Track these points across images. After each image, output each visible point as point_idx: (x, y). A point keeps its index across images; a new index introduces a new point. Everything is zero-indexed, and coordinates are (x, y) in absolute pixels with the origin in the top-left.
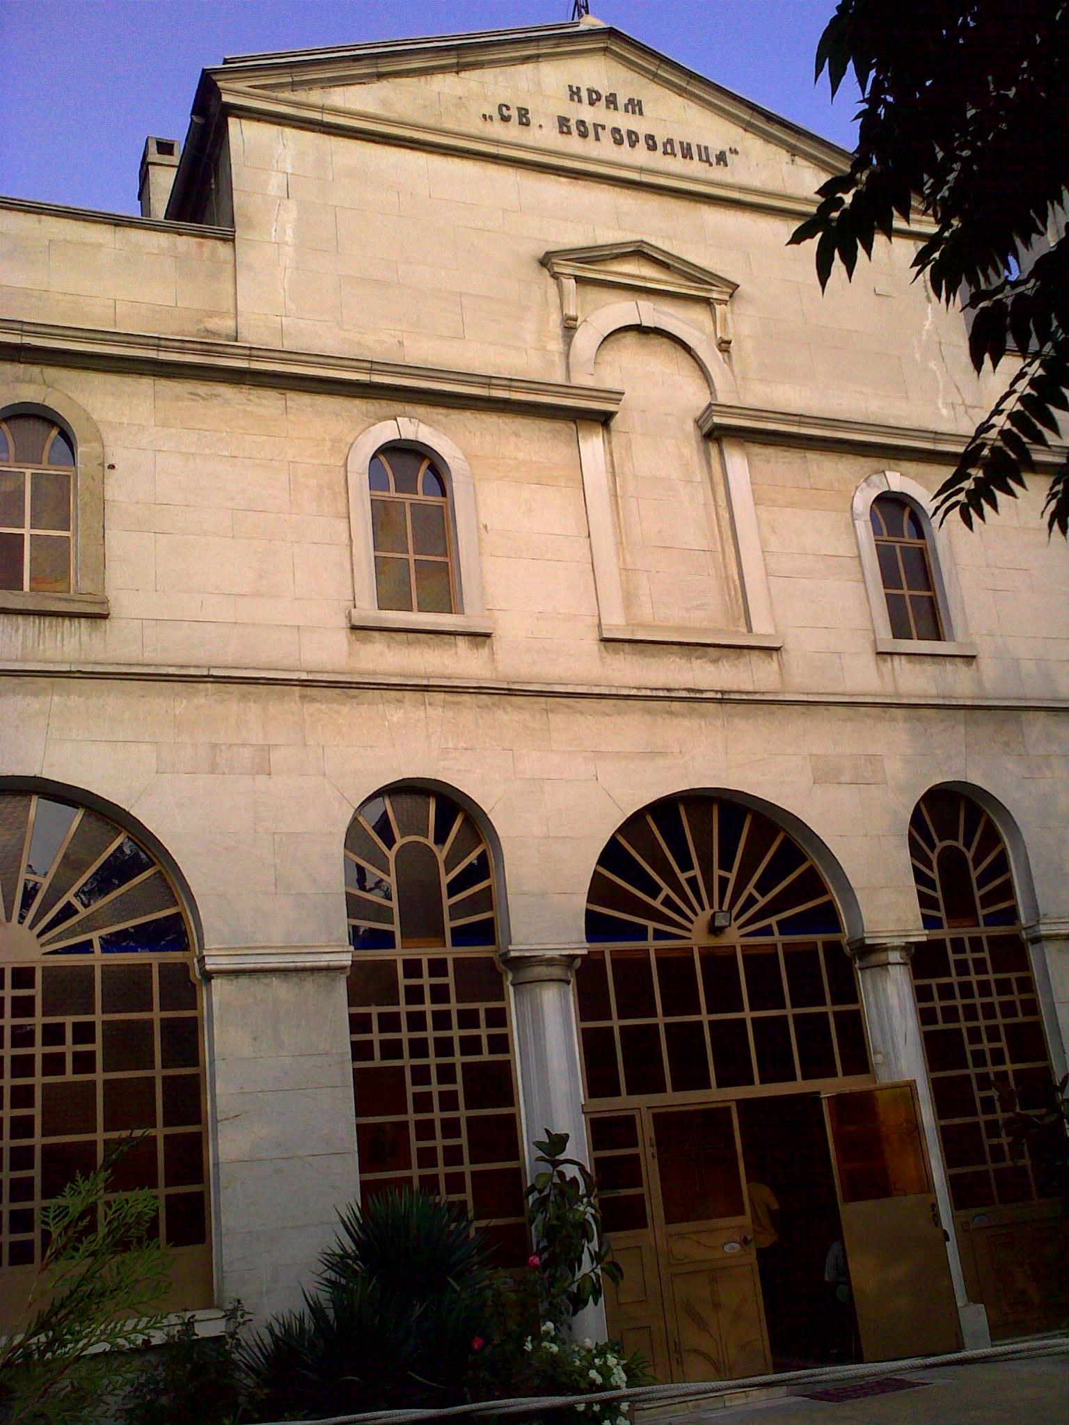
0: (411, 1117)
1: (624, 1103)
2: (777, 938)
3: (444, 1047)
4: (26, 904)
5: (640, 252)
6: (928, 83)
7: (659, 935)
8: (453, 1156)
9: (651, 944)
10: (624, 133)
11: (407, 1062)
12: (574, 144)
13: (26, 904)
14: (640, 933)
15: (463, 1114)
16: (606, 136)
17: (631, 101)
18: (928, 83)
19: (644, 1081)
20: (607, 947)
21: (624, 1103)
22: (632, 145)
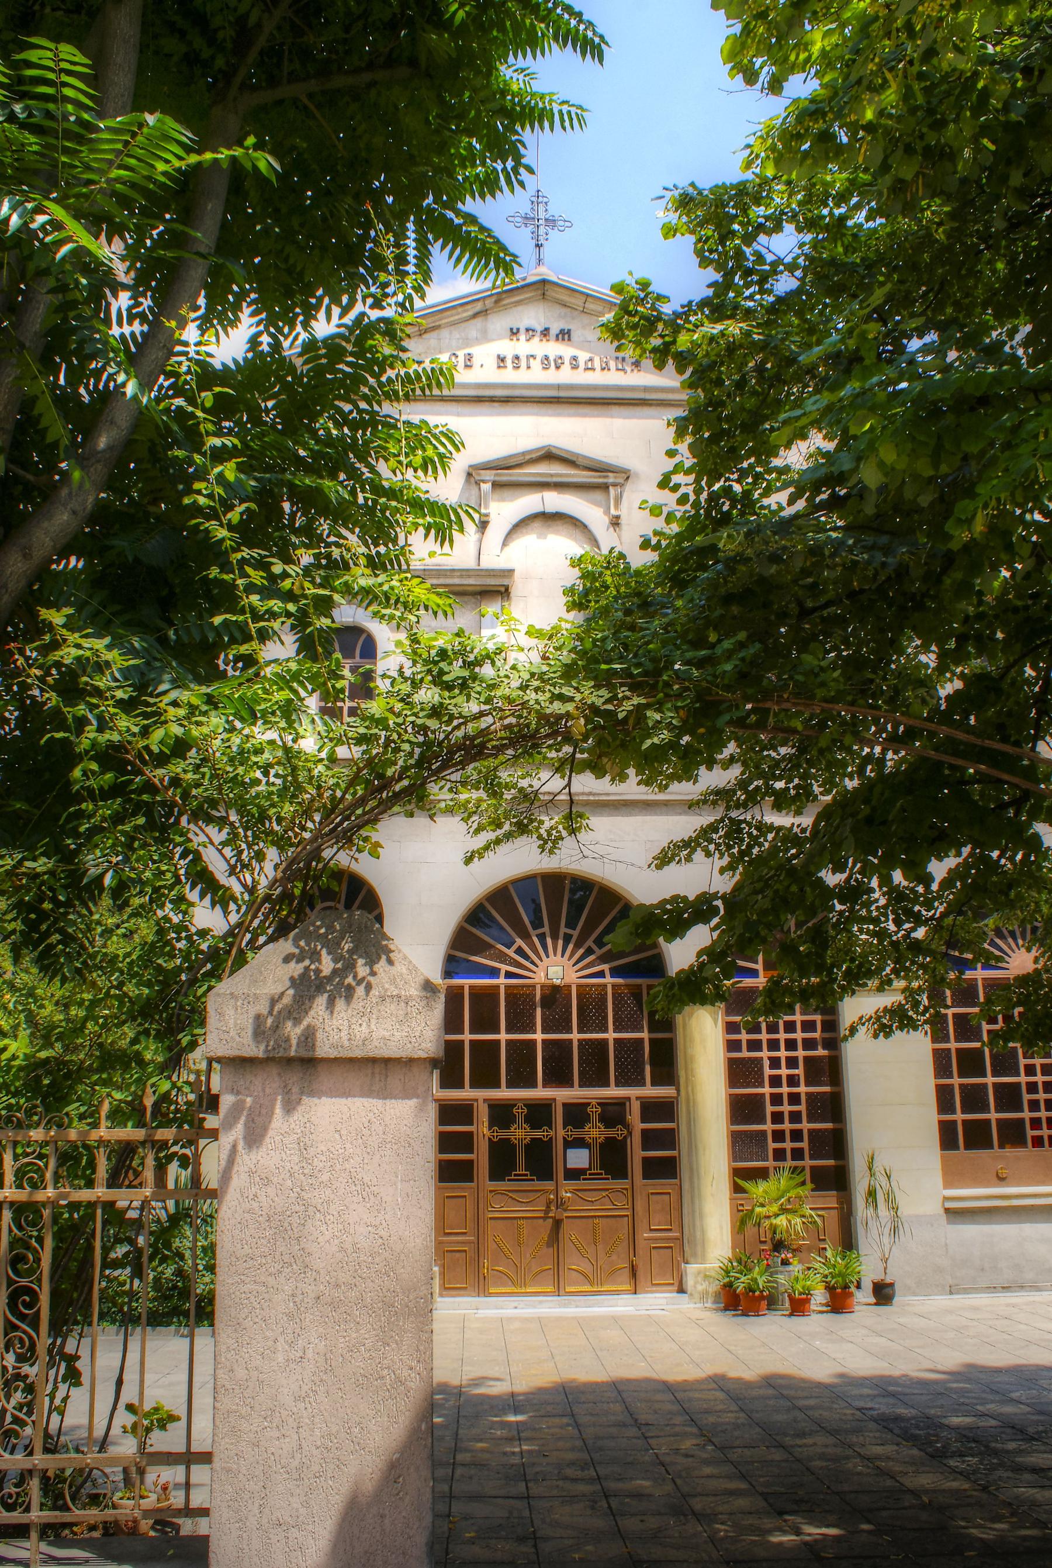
0: (767, 1090)
1: (466, 1094)
2: (608, 980)
3: (773, 1045)
4: (526, 957)
5: (549, 456)
6: (256, 261)
7: (509, 975)
8: (795, 1117)
9: (501, 981)
10: (552, 359)
11: (765, 1054)
12: (510, 376)
13: (526, 957)
14: (494, 973)
15: (802, 1089)
16: (536, 364)
17: (562, 332)
18: (256, 261)
19: (485, 1077)
20: (467, 982)
21: (466, 1094)
22: (558, 368)
